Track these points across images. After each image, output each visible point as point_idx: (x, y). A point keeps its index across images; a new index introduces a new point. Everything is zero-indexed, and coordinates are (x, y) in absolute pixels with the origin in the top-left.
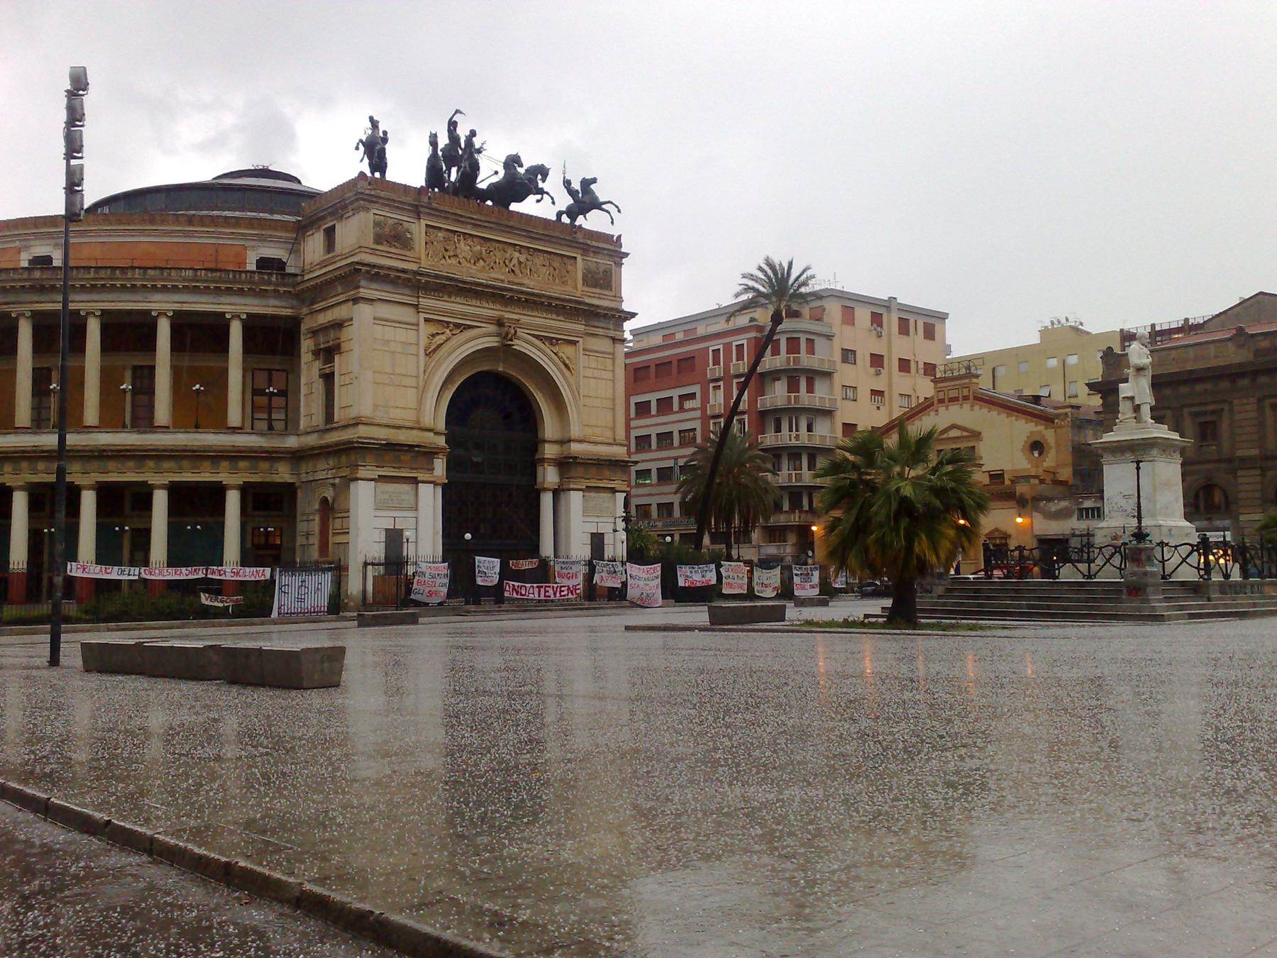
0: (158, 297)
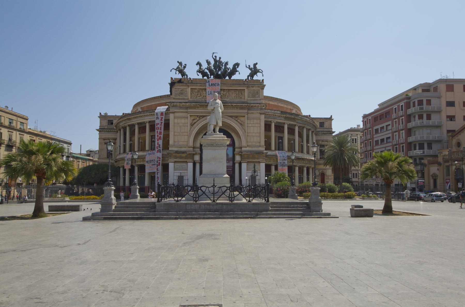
0: (146, 118)
